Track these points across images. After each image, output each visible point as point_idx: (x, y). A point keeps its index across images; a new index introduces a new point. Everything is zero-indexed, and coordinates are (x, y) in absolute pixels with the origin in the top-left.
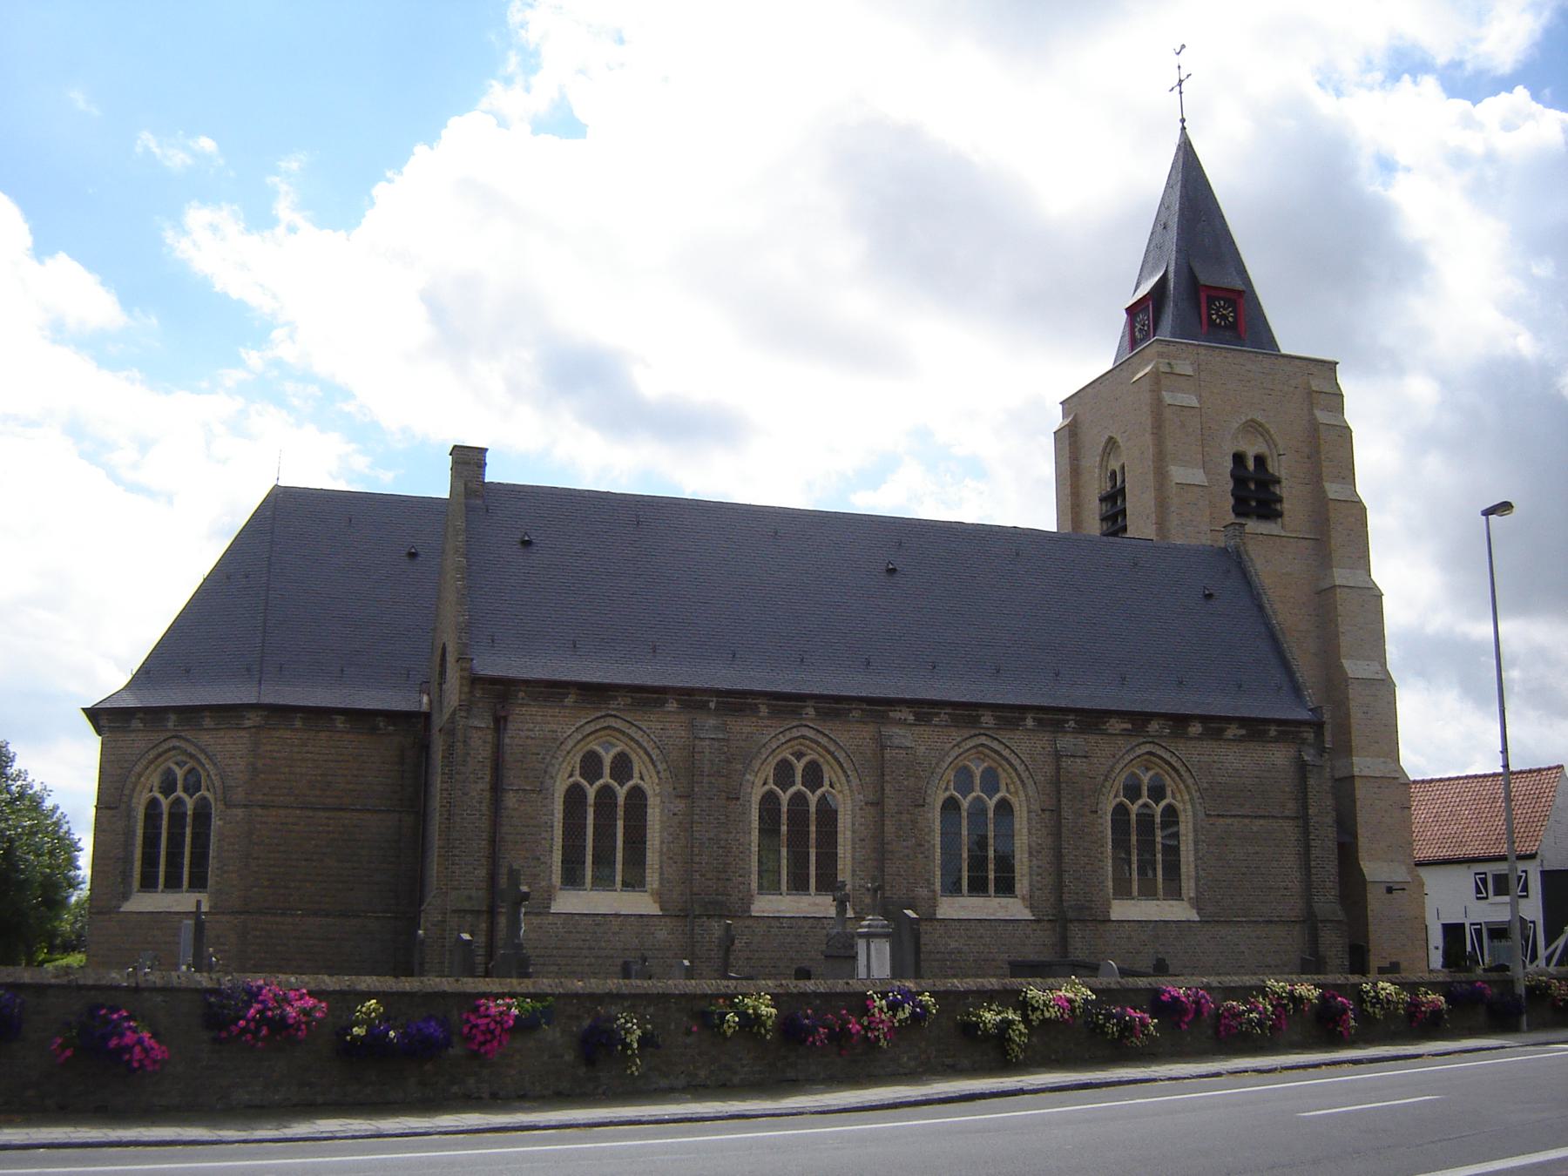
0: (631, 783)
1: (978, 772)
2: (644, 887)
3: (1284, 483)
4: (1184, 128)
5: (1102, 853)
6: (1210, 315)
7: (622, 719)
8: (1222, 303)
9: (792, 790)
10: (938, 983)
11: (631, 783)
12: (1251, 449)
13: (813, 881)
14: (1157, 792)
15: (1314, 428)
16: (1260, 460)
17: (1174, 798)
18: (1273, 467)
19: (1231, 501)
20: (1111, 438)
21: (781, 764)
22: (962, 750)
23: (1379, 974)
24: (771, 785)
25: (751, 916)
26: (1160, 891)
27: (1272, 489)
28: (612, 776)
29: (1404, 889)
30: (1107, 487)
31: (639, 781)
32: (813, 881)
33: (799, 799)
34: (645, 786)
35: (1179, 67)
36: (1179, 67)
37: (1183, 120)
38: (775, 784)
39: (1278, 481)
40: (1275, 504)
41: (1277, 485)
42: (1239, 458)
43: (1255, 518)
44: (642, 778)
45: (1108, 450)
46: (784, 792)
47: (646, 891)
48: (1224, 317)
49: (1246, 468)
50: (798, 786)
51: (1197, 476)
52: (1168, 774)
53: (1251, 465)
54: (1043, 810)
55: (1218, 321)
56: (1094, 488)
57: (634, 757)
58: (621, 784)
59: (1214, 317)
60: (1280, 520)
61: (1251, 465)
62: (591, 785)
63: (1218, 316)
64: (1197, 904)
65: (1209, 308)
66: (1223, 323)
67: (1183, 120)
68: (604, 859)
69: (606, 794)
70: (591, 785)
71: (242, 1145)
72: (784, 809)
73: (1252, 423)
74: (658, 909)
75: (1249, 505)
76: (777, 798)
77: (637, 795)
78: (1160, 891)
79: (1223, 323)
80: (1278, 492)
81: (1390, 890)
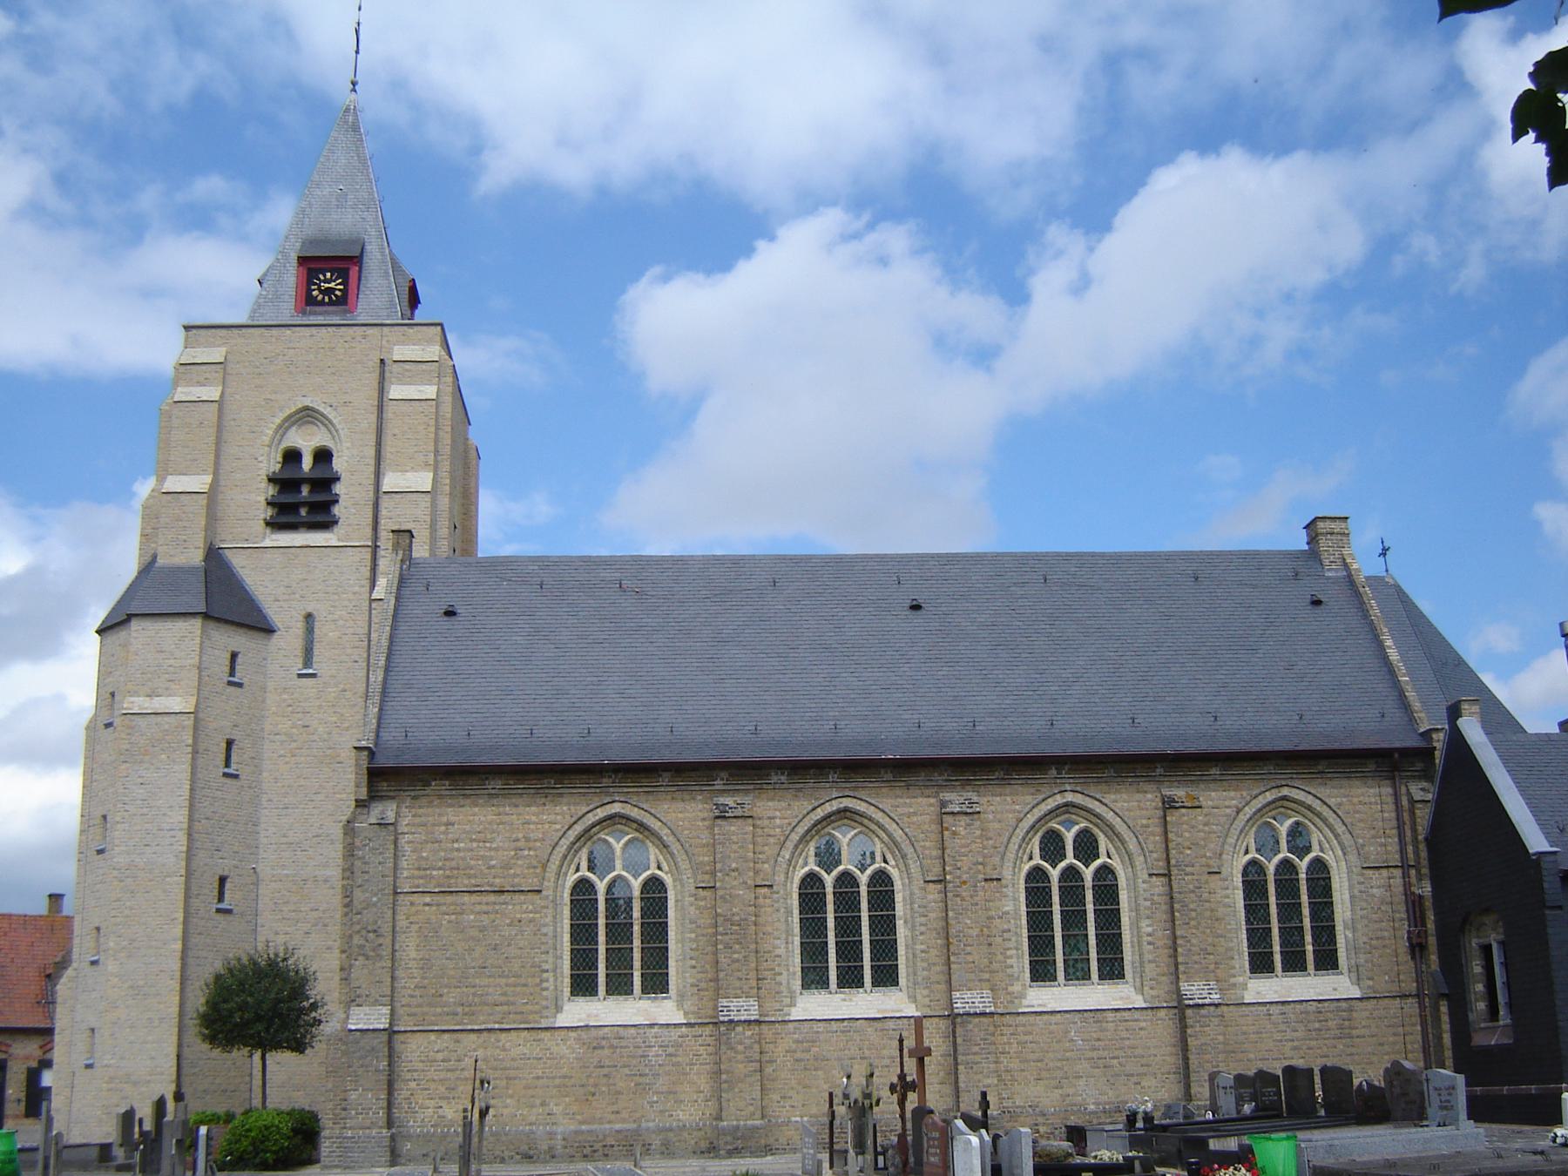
0: (1098, 862)
1: (1069, 837)
2: (668, 993)
5: (1077, 926)
7: (867, 801)
9: (1063, 865)
11: (1098, 862)
12: (306, 441)
13: (1277, 958)
14: (1086, 847)
17: (885, 861)
21: (1088, 835)
23: (1351, 1072)
24: (1037, 860)
28: (1076, 857)
31: (883, 865)
32: (1277, 958)
33: (1071, 874)
34: (1115, 864)
35: (360, 9)
36: (360, 9)
38: (1289, 851)
44: (885, 861)
46: (1087, 867)
47: (670, 998)
48: (330, 291)
50: (1070, 859)
51: (423, 480)
52: (1098, 827)
54: (1151, 875)
57: (1096, 831)
58: (636, 877)
59: (315, 293)
61: (307, 463)
62: (1054, 867)
63: (321, 291)
64: (1357, 975)
66: (327, 299)
68: (620, 959)
69: (1071, 874)
70: (1054, 867)
72: (1303, 876)
74: (682, 1016)
76: (821, 881)
77: (1319, 866)
79: (327, 299)
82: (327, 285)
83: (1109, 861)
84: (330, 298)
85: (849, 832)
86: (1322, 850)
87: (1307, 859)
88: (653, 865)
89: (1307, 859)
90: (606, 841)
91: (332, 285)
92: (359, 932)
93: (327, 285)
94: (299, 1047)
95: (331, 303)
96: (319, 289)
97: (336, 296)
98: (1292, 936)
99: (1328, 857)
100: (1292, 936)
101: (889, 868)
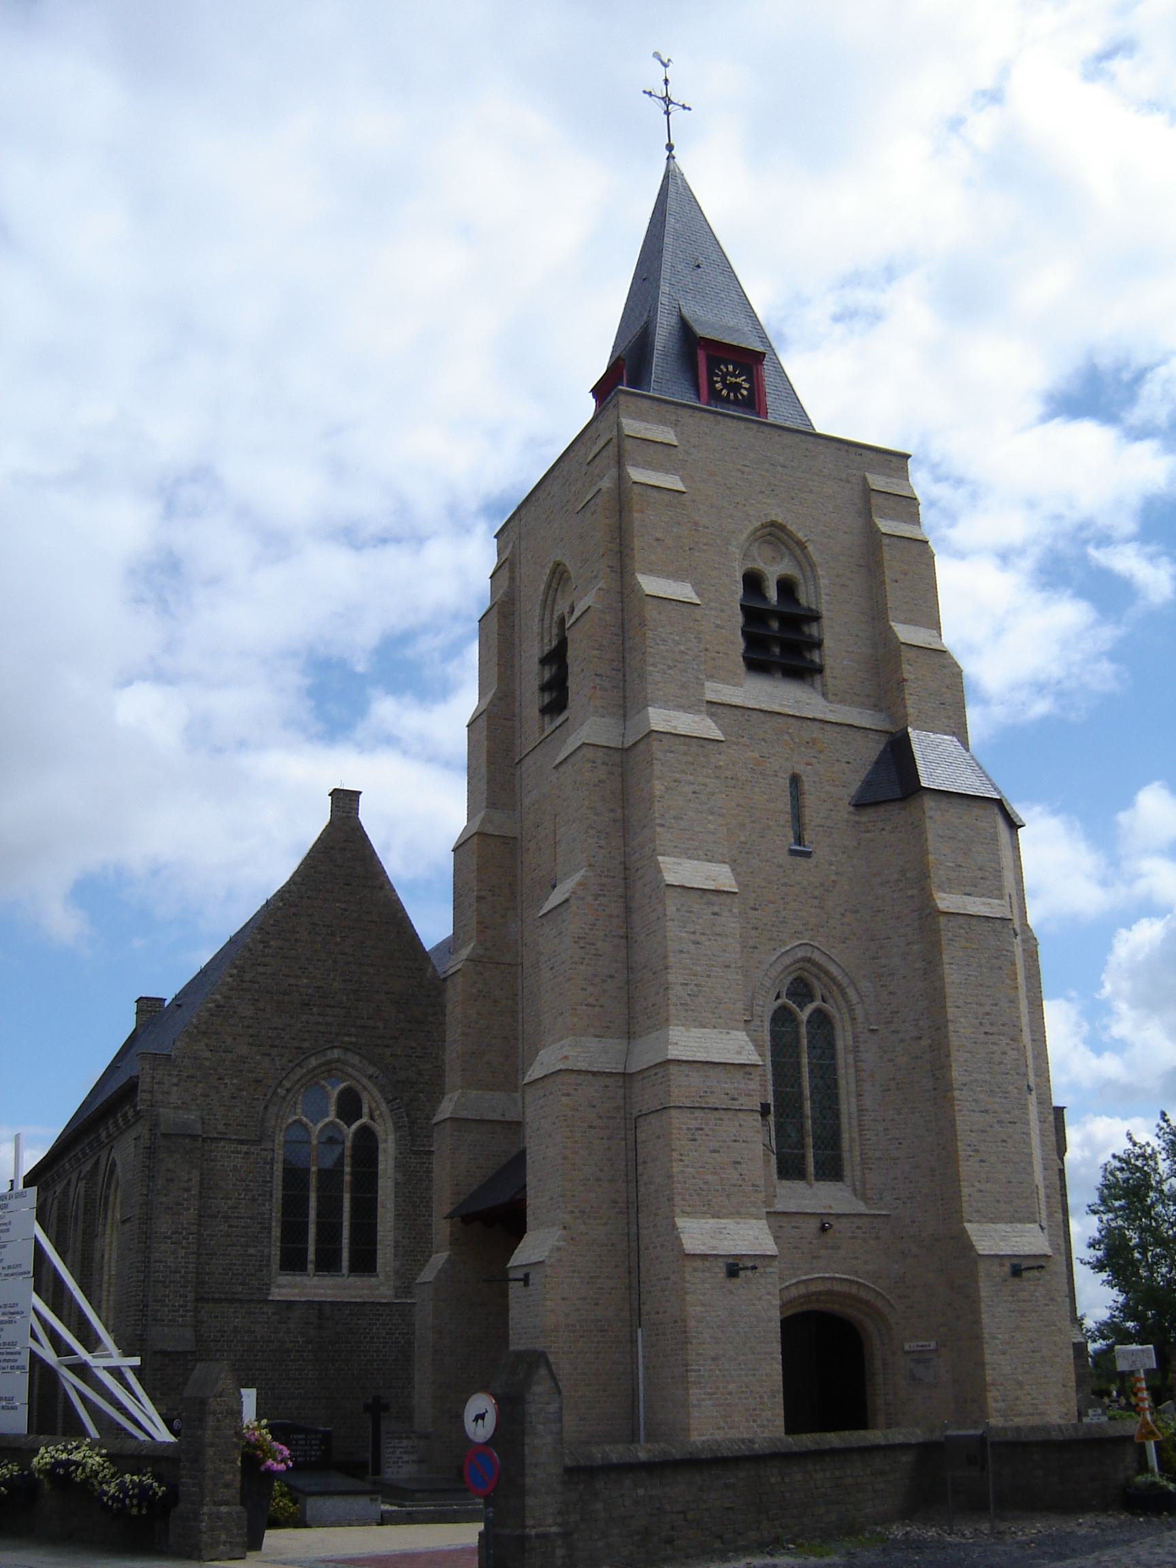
3: (825, 622)
4: (670, 158)
6: (712, 384)
8: (731, 368)
10: (275, 1465)
12: (773, 571)
15: (873, 541)
16: (787, 587)
18: (805, 597)
19: (740, 644)
20: (558, 564)
22: (304, 1070)
25: (267, 1302)
26: (811, 1168)
27: (808, 656)
29: (1042, 1267)
30: (551, 644)
37: (670, 147)
39: (815, 617)
40: (810, 651)
41: (815, 624)
42: (753, 582)
43: (779, 675)
45: (554, 585)
49: (764, 598)
53: (772, 594)
55: (724, 392)
56: (532, 649)
58: (802, 1007)
60: (818, 678)
61: (772, 594)
63: (725, 386)
65: (711, 374)
67: (670, 147)
71: (157, 1424)
73: (807, 965)
75: (767, 626)
78: (811, 1168)
80: (817, 660)
81: (1017, 1271)
82: (733, 380)
83: (372, 1122)
84: (736, 396)
85: (338, 1084)
86: (372, 1118)
87: (810, 1008)
88: (780, 1001)
89: (810, 1008)
90: (323, 1087)
91: (739, 380)
92: (271, 1214)
93: (733, 380)
94: (779, 1178)
95: (737, 403)
96: (723, 381)
97: (741, 394)
98: (329, 1233)
99: (378, 1128)
100: (329, 1233)
101: (376, 1125)
